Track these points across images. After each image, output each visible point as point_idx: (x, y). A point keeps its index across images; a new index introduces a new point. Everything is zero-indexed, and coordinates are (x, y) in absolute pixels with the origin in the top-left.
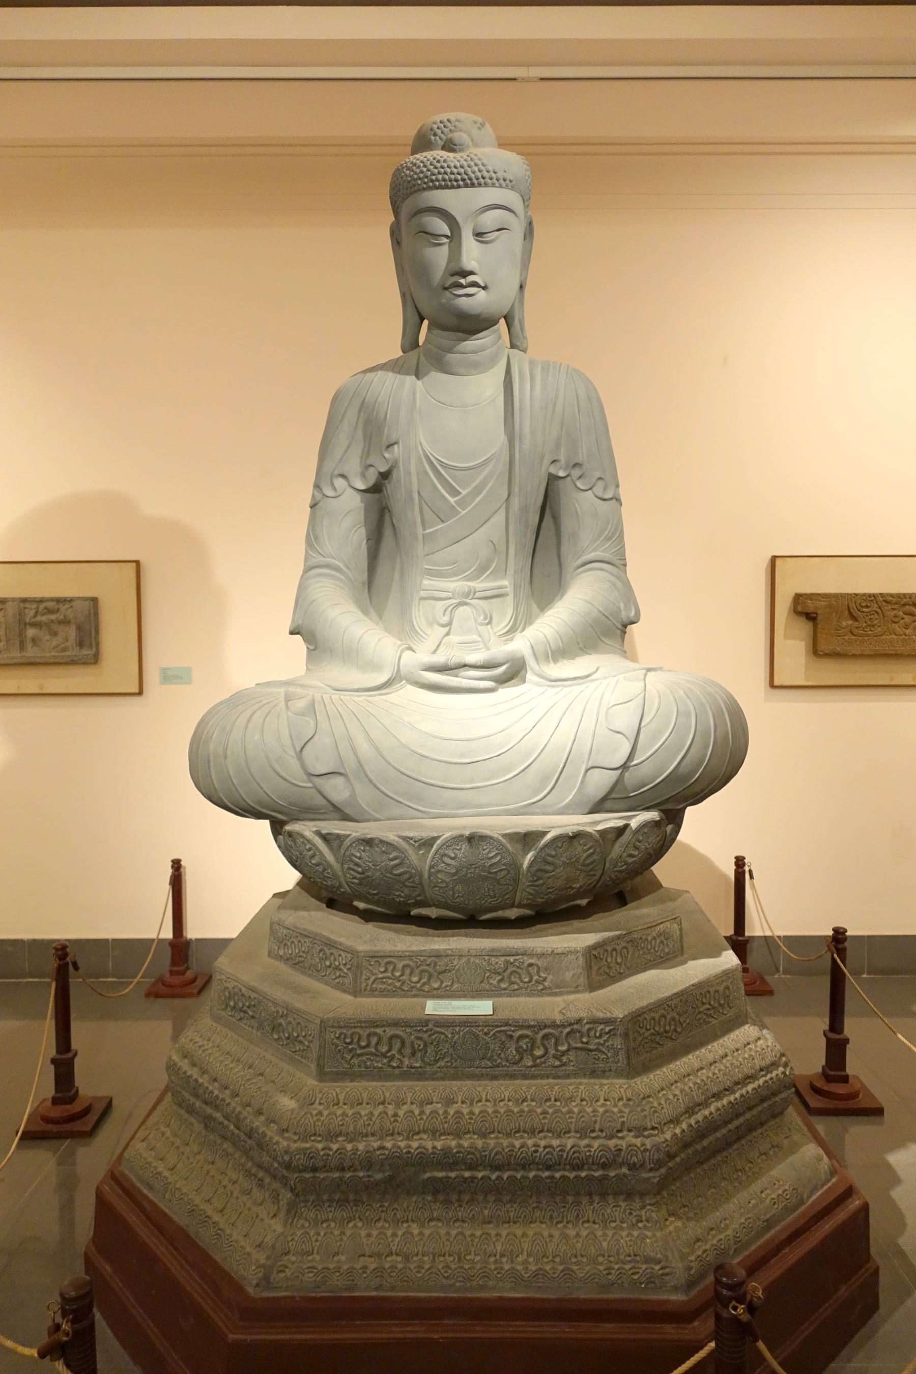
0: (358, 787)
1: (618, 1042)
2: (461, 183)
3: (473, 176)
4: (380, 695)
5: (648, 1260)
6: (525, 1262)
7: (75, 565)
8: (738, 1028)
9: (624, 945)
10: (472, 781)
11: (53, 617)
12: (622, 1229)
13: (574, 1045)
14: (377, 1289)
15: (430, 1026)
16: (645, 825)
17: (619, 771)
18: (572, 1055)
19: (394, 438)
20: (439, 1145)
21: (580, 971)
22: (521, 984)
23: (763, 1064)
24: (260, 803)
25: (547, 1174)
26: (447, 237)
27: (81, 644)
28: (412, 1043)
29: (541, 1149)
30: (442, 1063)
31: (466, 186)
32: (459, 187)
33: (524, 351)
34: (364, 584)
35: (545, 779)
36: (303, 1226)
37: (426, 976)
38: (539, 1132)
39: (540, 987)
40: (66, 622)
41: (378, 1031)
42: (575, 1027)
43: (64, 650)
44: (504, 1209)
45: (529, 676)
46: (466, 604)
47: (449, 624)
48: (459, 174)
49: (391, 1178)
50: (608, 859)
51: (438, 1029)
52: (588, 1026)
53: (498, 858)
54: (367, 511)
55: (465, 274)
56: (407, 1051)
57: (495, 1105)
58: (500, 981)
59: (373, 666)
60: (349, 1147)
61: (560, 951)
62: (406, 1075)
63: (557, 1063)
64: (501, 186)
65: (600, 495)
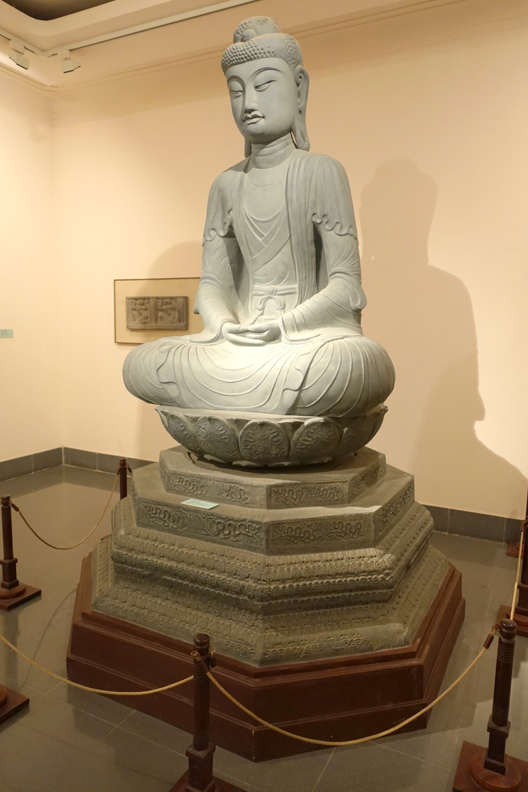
0: (182, 390)
1: (262, 535)
2: (245, 59)
3: (250, 54)
4: (211, 345)
5: (247, 644)
6: (195, 628)
7: (179, 280)
8: (364, 548)
9: (301, 489)
10: (233, 392)
11: (169, 306)
12: (244, 627)
13: (242, 532)
14: (134, 621)
15: (181, 509)
16: (314, 424)
17: (298, 392)
18: (241, 537)
19: (230, 208)
20: (169, 564)
21: (264, 497)
22: (236, 499)
23: (367, 569)
24: (143, 395)
25: (212, 590)
26: (241, 91)
27: (180, 320)
28: (173, 516)
29: (209, 577)
30: (185, 528)
31: (248, 60)
32: (245, 62)
33: (307, 149)
34: (231, 287)
35: (266, 393)
36: (118, 587)
37: (195, 486)
38: (212, 569)
39: (245, 502)
40: (174, 309)
41: (161, 507)
42: (243, 523)
43: (173, 323)
44: (196, 603)
45: (283, 338)
46: (272, 298)
47: (263, 309)
48: (243, 54)
49: (151, 575)
50: (291, 441)
51: (184, 511)
52: (249, 523)
53: (224, 431)
54: (228, 247)
55: (250, 111)
56: (171, 520)
57: (199, 552)
58: (227, 496)
59: (212, 331)
60: (135, 556)
61: (255, 485)
62: (170, 531)
63: (235, 540)
64: (267, 57)
65: (338, 233)
